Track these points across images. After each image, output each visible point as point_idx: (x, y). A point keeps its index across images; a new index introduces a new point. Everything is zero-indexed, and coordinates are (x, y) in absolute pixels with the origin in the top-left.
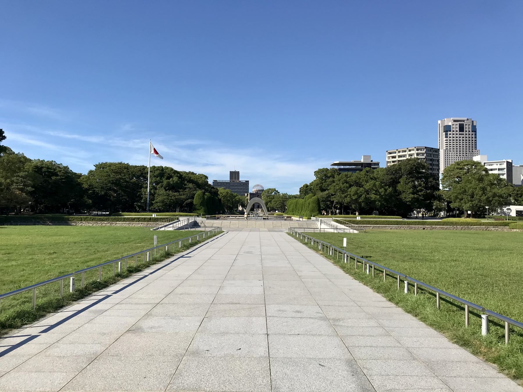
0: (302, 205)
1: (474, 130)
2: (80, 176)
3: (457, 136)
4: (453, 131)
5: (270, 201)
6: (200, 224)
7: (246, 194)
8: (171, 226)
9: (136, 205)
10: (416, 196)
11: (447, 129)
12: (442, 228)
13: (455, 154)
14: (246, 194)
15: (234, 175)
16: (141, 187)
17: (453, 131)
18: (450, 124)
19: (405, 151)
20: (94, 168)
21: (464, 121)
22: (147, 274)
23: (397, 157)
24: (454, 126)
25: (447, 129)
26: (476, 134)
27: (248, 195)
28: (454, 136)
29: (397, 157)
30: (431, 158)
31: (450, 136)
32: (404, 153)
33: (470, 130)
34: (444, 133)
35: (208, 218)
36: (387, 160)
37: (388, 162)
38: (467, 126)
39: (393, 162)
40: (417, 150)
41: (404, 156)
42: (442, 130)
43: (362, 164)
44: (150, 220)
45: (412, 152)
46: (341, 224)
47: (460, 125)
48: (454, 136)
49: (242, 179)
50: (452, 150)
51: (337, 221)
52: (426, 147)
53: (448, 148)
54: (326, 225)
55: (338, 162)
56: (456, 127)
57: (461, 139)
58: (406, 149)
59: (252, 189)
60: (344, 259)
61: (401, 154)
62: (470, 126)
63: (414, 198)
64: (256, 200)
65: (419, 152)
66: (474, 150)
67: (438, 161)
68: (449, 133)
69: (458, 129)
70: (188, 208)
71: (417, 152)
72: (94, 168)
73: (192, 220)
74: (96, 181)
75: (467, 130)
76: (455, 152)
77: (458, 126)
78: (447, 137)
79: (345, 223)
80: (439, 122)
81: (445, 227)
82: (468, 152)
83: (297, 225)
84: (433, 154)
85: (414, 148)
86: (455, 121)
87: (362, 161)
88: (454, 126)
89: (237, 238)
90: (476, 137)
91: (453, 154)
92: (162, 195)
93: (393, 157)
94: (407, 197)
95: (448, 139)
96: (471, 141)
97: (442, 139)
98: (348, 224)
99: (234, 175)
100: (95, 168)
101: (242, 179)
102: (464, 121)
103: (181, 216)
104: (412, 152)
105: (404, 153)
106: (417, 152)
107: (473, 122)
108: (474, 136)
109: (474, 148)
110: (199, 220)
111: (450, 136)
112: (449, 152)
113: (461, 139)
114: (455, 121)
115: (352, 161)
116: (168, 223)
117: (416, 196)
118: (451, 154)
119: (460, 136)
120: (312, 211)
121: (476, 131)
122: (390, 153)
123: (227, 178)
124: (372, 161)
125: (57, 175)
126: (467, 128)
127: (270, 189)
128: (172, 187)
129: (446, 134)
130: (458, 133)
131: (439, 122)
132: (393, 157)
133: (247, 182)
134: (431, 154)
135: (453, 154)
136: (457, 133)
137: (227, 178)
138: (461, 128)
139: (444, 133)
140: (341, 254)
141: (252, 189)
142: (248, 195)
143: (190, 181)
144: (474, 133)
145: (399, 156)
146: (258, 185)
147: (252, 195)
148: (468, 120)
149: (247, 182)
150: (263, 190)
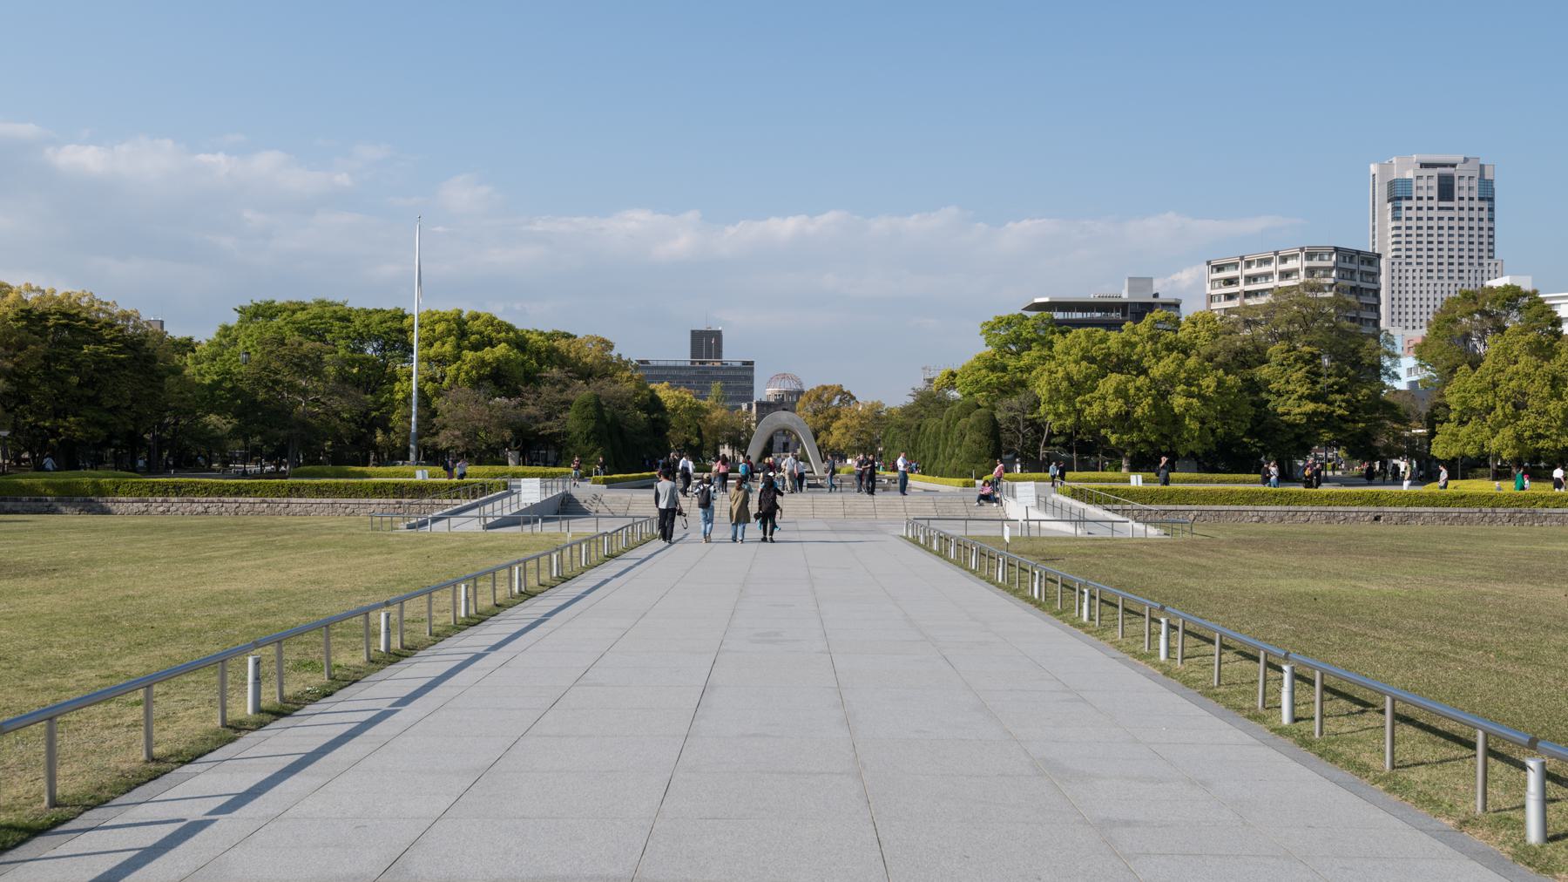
0: (937, 433)
1: (1487, 196)
2: (187, 346)
3: (1431, 214)
4: (1420, 198)
5: (827, 428)
6: (585, 506)
7: (744, 406)
8: (475, 512)
9: (1082, 402)
10: (1323, 407)
11: (1398, 194)
12: (1441, 516)
13: (1424, 274)
14: (744, 406)
15: (706, 342)
16: (394, 378)
17: (1420, 198)
18: (1409, 175)
19: (1268, 261)
20: (233, 319)
21: (1454, 166)
22: (196, 812)
23: (1242, 281)
24: (1421, 183)
25: (1398, 194)
26: (1491, 210)
27: (750, 408)
28: (1420, 214)
29: (1242, 281)
30: (1353, 284)
31: (1409, 214)
32: (1265, 269)
33: (1475, 194)
34: (1390, 206)
35: (610, 483)
36: (1209, 291)
37: (1211, 298)
38: (1464, 183)
39: (1230, 297)
40: (1310, 256)
41: (1268, 276)
42: (1382, 192)
43: (1123, 307)
44: (399, 491)
45: (1291, 264)
46: (1097, 502)
47: (1441, 177)
48: (1420, 214)
49: (732, 354)
50: (1414, 260)
51: (1074, 494)
52: (1336, 249)
53: (1403, 253)
54: (1026, 503)
55: (1046, 300)
56: (1429, 186)
57: (1444, 223)
58: (1271, 255)
59: (765, 390)
60: (1080, 608)
61: (1254, 270)
62: (1475, 183)
63: (1315, 413)
64: (782, 418)
65: (1316, 263)
66: (1485, 261)
67: (1376, 293)
68: (1405, 204)
69: (1434, 193)
70: (538, 448)
71: (1306, 264)
72: (233, 319)
73: (557, 489)
74: (243, 363)
75: (1464, 194)
76: (1425, 267)
77: (1434, 183)
78: (1399, 219)
79: (1108, 501)
80: (1374, 168)
81: (1454, 510)
82: (1466, 267)
83: (930, 507)
84: (1358, 267)
85: (1297, 251)
86: (1424, 165)
87: (1125, 296)
88: (1421, 183)
89: (662, 617)
90: (1491, 219)
91: (1417, 274)
92: (464, 409)
93: (1230, 282)
94: (1294, 408)
95: (1403, 223)
96: (1475, 232)
97: (1383, 224)
98: (1116, 502)
99: (706, 342)
100: (237, 316)
101: (732, 354)
102: (1454, 166)
103: (525, 475)
104: (1291, 264)
105: (1265, 269)
106: (1306, 264)
107: (1482, 167)
108: (1484, 215)
109: (1485, 254)
110: (584, 491)
111: (1409, 214)
112: (1404, 267)
113: (1444, 223)
114: (1424, 165)
115: (1091, 296)
116: (467, 503)
117: (1323, 407)
118: (1410, 274)
119: (1442, 214)
120: (976, 459)
121: (1491, 199)
122: (1220, 268)
123: (679, 353)
124: (1156, 296)
125: (100, 342)
126: (1462, 188)
127: (825, 388)
128: (498, 379)
129: (1396, 209)
130: (1434, 203)
131: (1374, 168)
132: (1230, 282)
133: (749, 365)
134: (1352, 272)
135: (1417, 274)
136: (1431, 203)
137: (679, 353)
138: (1446, 189)
139: (1390, 206)
140: (1068, 593)
141: (765, 390)
142: (750, 408)
143: (562, 361)
144: (1485, 205)
145: (1250, 279)
146: (784, 376)
147: (765, 407)
148: (1466, 160)
149: (749, 365)
150: (800, 393)
